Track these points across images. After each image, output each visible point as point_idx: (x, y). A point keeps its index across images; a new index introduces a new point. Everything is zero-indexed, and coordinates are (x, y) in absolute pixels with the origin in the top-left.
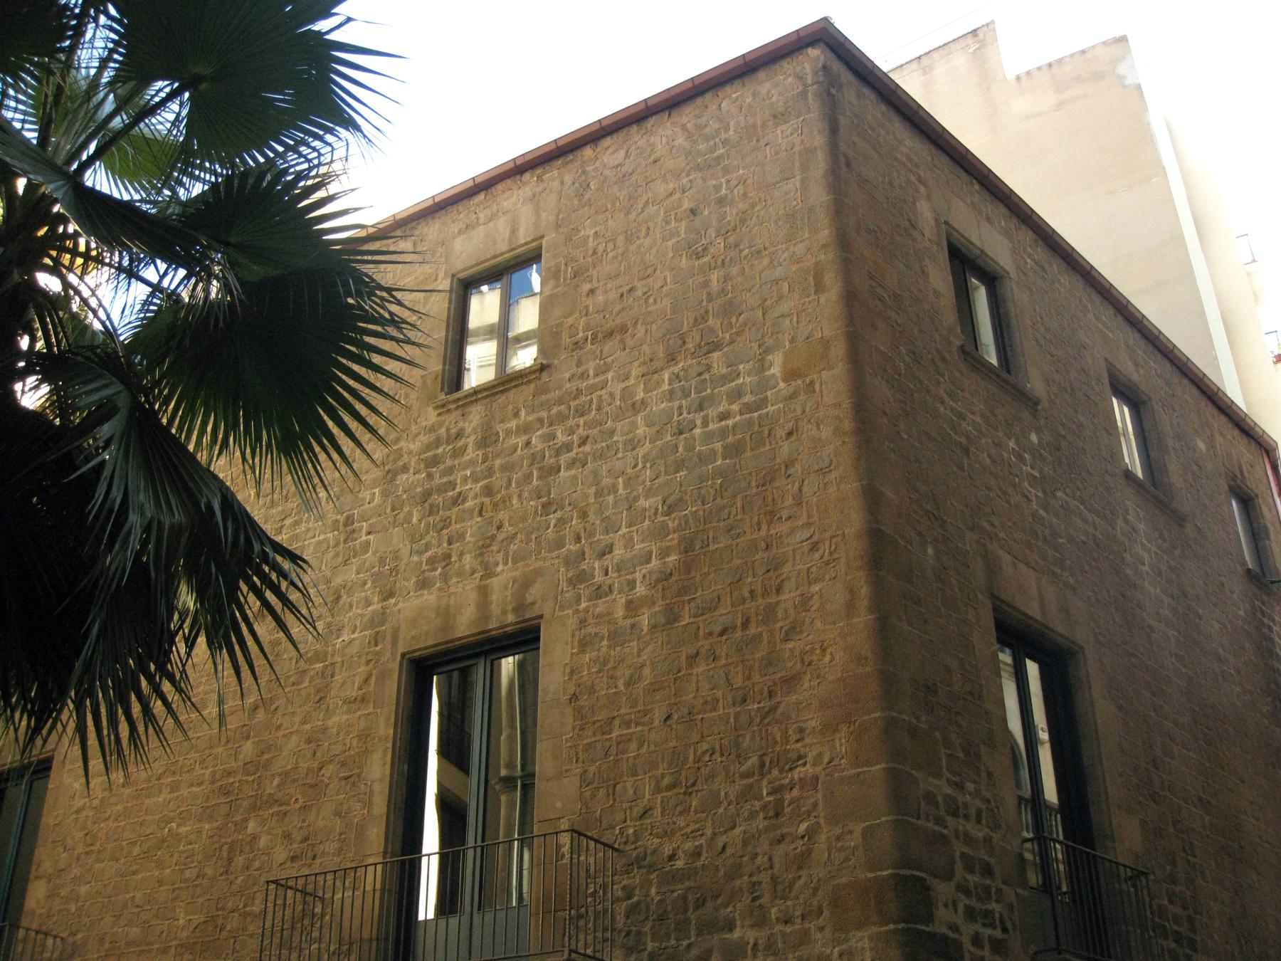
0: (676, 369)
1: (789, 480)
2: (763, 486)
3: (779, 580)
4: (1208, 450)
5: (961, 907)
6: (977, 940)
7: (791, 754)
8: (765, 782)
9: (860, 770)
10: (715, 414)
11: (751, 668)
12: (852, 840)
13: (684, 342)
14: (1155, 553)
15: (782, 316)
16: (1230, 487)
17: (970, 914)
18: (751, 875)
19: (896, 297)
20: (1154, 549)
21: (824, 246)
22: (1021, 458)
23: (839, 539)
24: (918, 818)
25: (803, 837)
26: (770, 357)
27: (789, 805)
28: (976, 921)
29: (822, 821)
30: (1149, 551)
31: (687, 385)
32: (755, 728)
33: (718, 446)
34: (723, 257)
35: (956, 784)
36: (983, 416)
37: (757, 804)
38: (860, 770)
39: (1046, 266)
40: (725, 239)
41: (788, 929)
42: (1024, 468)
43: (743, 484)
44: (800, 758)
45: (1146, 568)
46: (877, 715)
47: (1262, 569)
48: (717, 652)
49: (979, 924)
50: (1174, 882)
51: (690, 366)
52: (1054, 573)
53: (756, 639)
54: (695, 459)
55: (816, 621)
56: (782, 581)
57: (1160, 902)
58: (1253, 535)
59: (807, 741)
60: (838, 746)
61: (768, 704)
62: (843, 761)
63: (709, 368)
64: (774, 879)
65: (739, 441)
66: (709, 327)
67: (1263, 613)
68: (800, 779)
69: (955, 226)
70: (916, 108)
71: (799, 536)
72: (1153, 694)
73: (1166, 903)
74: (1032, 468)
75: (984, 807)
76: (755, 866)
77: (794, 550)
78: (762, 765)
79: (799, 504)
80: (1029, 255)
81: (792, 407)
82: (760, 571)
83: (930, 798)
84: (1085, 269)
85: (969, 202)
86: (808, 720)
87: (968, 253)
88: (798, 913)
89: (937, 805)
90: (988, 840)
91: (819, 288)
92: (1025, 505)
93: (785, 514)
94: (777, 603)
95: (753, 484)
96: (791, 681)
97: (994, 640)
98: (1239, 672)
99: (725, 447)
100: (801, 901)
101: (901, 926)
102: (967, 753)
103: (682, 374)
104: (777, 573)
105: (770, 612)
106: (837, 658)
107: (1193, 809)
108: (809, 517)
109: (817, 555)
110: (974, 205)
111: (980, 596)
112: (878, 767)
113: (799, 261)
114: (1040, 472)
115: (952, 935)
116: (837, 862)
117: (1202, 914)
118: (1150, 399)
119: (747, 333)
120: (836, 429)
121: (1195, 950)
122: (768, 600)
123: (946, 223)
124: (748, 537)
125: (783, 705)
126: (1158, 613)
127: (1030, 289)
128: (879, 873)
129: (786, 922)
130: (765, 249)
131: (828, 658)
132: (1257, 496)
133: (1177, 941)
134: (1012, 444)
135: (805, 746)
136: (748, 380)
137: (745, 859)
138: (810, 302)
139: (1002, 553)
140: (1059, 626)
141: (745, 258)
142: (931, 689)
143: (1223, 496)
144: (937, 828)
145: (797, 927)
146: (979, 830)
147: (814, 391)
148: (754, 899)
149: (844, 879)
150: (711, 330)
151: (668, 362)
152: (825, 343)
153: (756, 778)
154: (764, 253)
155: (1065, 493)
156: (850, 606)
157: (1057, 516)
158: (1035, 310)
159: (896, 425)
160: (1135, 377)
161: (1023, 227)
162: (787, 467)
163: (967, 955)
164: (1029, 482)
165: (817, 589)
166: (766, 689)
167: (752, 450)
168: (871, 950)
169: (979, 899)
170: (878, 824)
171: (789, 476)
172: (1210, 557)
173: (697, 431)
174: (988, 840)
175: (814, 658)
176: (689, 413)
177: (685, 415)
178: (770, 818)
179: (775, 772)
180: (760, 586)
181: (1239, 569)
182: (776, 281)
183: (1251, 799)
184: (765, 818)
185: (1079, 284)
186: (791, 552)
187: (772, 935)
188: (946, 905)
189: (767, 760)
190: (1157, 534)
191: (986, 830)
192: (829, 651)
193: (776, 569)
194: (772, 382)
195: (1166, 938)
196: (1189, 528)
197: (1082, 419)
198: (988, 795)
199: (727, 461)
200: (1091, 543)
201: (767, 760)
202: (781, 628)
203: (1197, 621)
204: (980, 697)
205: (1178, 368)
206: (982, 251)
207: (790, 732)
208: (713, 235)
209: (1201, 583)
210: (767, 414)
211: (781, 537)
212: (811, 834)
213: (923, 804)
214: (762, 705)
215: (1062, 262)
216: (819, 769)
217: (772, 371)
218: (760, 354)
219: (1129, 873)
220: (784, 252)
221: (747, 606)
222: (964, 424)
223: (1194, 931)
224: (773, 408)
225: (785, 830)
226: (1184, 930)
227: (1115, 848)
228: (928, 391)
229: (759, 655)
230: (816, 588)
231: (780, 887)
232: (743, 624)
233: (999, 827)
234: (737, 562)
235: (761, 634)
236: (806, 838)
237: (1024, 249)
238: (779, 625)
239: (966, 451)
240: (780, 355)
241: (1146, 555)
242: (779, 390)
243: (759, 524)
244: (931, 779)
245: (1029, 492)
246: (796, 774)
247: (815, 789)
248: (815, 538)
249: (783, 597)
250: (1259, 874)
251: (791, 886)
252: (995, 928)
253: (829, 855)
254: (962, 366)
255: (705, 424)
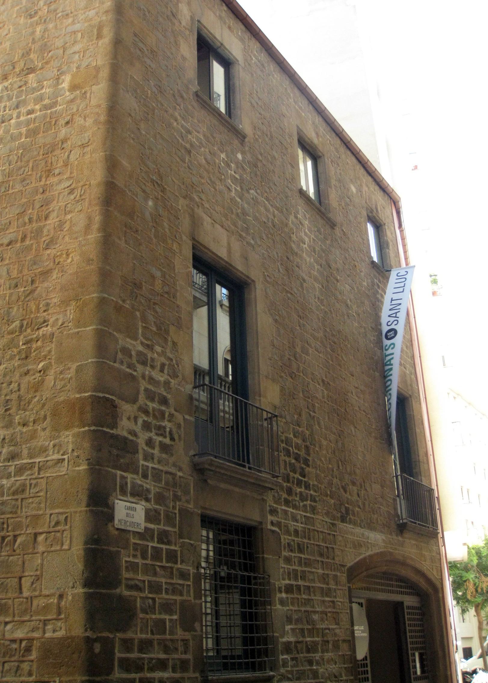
0: (6, 84)
1: (63, 151)
2: (47, 154)
3: (47, 212)
4: (357, 192)
5: (140, 422)
6: (150, 443)
7: (39, 320)
8: (22, 337)
9: (79, 330)
10: (25, 111)
11: (23, 265)
12: (69, 373)
13: (14, 68)
14: (313, 239)
15: (75, 53)
16: (368, 216)
17: (147, 426)
18: (6, 395)
19: (152, 51)
20: (312, 236)
21: (107, 12)
22: (228, 166)
23: (87, 186)
24: (115, 362)
25: (40, 371)
26: (63, 77)
27: (34, 351)
28: (151, 432)
29: (53, 361)
30: (309, 237)
31: (11, 94)
32: (20, 303)
33: (24, 130)
34: (45, 17)
35: (148, 346)
36: (204, 136)
37: (15, 350)
38: (79, 330)
39: (266, 65)
40: (49, 7)
41: (25, 429)
42: (229, 171)
43: (35, 153)
44: (45, 322)
45: (306, 246)
46: (94, 295)
47: (383, 264)
48: (5, 256)
49: (153, 433)
50: (299, 426)
51: (15, 82)
52: (241, 236)
53: (29, 248)
54: (9, 138)
55: (66, 237)
56: (49, 212)
57: (288, 435)
58: (380, 246)
59: (50, 312)
60: (68, 314)
61: (30, 288)
62: (70, 324)
63: (26, 83)
64: (20, 398)
65: (37, 127)
66: (30, 59)
67: (379, 287)
68: (43, 335)
69: (205, 24)
70: (245, 16)
71: (62, 186)
72: (300, 316)
73: (292, 437)
74: (235, 172)
75: (167, 363)
76: (10, 389)
77: (59, 194)
78: (22, 326)
79: (66, 165)
80: (255, 55)
81: (72, 107)
82: (37, 206)
83: (126, 351)
84: (269, 46)
85: (218, 14)
86: (52, 298)
87: (212, 44)
88: (32, 419)
89: (130, 356)
90: (167, 384)
91: (99, 36)
92: (226, 193)
93: (57, 172)
94: (44, 226)
95: (41, 153)
96: (46, 273)
97: (191, 266)
98: (359, 315)
99: (28, 131)
100: (34, 411)
101: (92, 428)
102: (159, 329)
103: (9, 86)
104: (47, 207)
105: (39, 232)
106: (75, 260)
107: (318, 386)
108: (71, 173)
109: (72, 197)
110: (220, 17)
111: (184, 238)
112: (90, 328)
113: (91, 20)
114: (240, 176)
115: (130, 437)
116: (58, 387)
117: (315, 445)
118: (324, 155)
119: (52, 62)
120: (95, 120)
121: (308, 466)
122: (39, 224)
123: (199, 21)
124: (33, 185)
125: (39, 288)
126: (310, 273)
127: (252, 75)
128: (83, 394)
129: (24, 425)
130: (71, 13)
131: (69, 260)
132: (385, 224)
133: (296, 459)
134: (223, 156)
135: (48, 315)
136: (48, 90)
137: (4, 385)
138: (92, 45)
139: (205, 217)
140: (239, 265)
141: (59, 18)
142: (138, 286)
143: (362, 219)
144: (128, 370)
145: (31, 428)
146: (162, 377)
147: (86, 98)
148: (6, 410)
149: (61, 398)
150: (32, 61)
151: (3, 80)
152: (97, 69)
153: (17, 334)
154: (70, 15)
155: (256, 192)
156: (88, 228)
157: (248, 204)
158: (253, 86)
159: (137, 124)
160: (315, 141)
161: (253, 39)
162: (62, 143)
163: (140, 451)
164: (231, 180)
165: (69, 217)
166: (30, 279)
167: (43, 132)
168: (73, 443)
169: (155, 417)
170: (87, 364)
171: (63, 149)
172: (349, 250)
173: (13, 121)
174: (167, 384)
175: (61, 260)
176: (10, 110)
177: (7, 111)
178: (22, 359)
179: (29, 331)
180: (35, 215)
181: (367, 259)
182: (75, 32)
183: (357, 386)
184: (19, 359)
185: (287, 83)
186: (57, 195)
187: (14, 433)
188: (129, 419)
189: (25, 323)
190: (316, 229)
191: (166, 377)
192: (71, 256)
193: (47, 205)
194: (63, 92)
195: (289, 456)
196: (337, 230)
197: (275, 154)
198: (171, 356)
199: (28, 139)
200: (270, 224)
201: (25, 323)
202: (44, 241)
203: (335, 282)
204: (174, 297)
205: (344, 143)
206: (222, 44)
207: (41, 306)
208: (42, 5)
209: (341, 262)
210: (56, 111)
211: (52, 186)
212: (44, 371)
213: (119, 353)
214: (26, 289)
215: (277, 65)
216: (55, 329)
217: (63, 85)
218: (58, 75)
219: (270, 415)
220: (82, 15)
221: (26, 227)
222: (190, 136)
223: (309, 455)
224: (60, 107)
225: (30, 367)
226: (302, 453)
227: (260, 400)
228: (167, 111)
229: (28, 258)
230: (69, 217)
231: (22, 403)
232: (22, 239)
233: (177, 376)
234: (24, 200)
235: (32, 244)
236: (42, 373)
237: (252, 52)
238: (44, 239)
239: (189, 152)
240: (70, 76)
241: (307, 239)
242: (66, 97)
243: (41, 178)
244: (128, 340)
245: (231, 186)
246: (41, 332)
247: (51, 342)
248: (72, 187)
249: (48, 222)
250: (355, 427)
251: (29, 403)
252: (165, 437)
253: (55, 383)
254: (195, 104)
255: (18, 117)
